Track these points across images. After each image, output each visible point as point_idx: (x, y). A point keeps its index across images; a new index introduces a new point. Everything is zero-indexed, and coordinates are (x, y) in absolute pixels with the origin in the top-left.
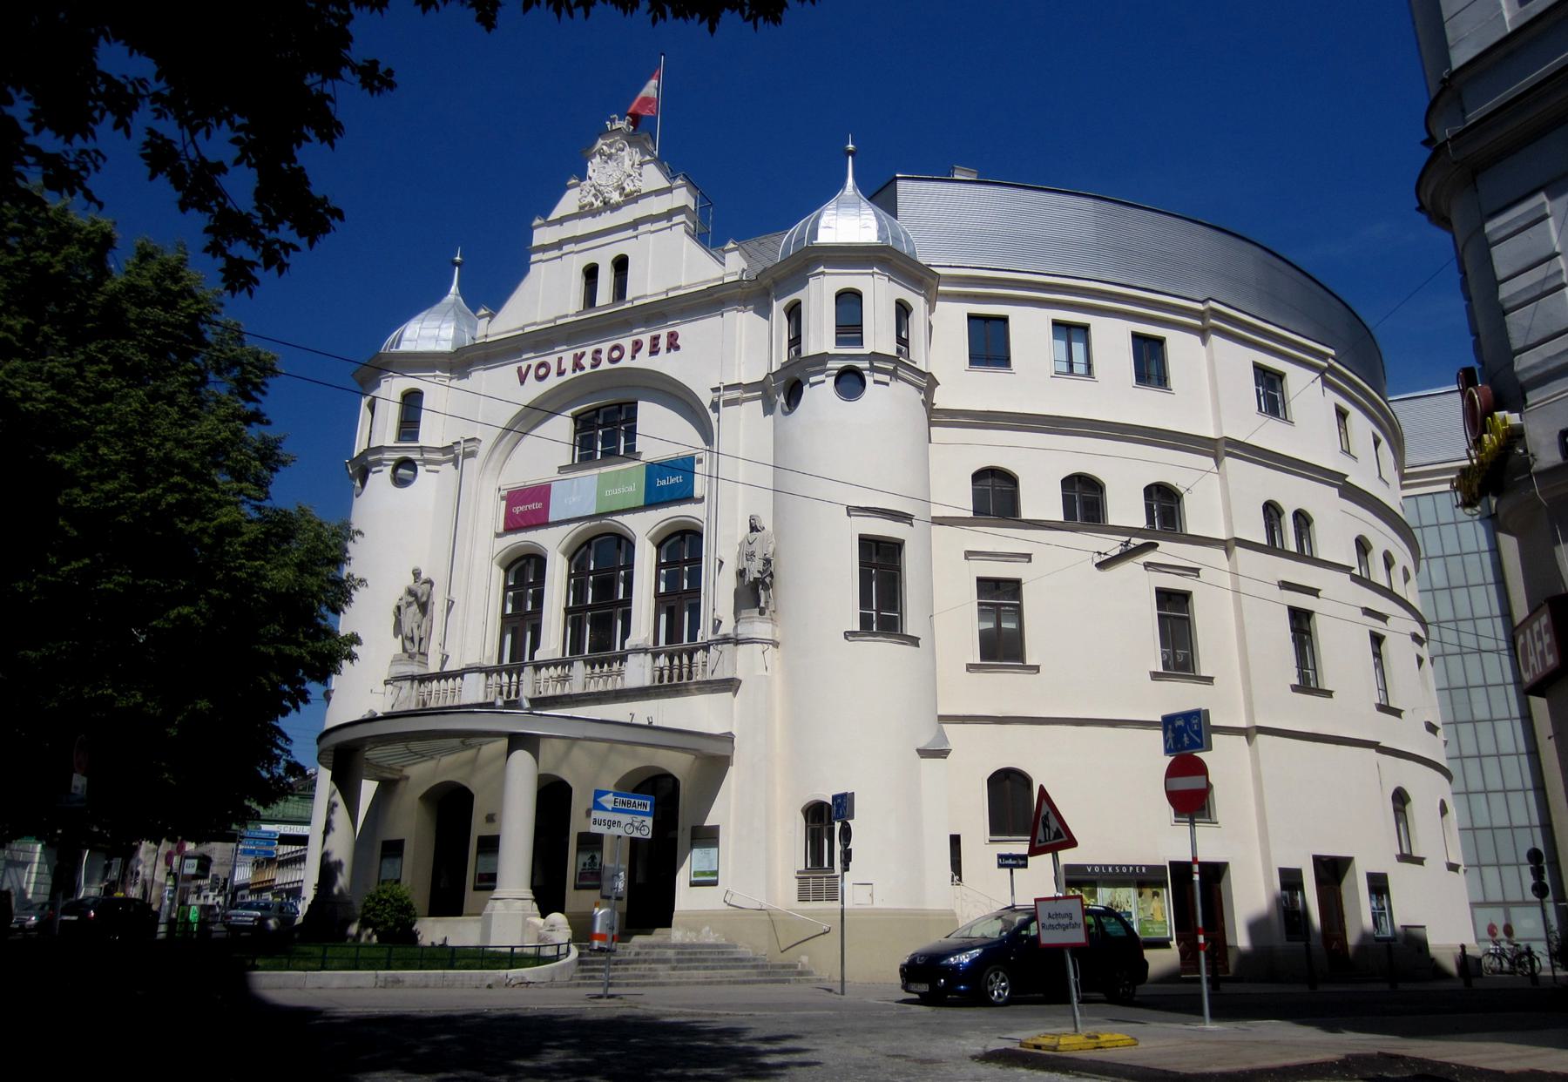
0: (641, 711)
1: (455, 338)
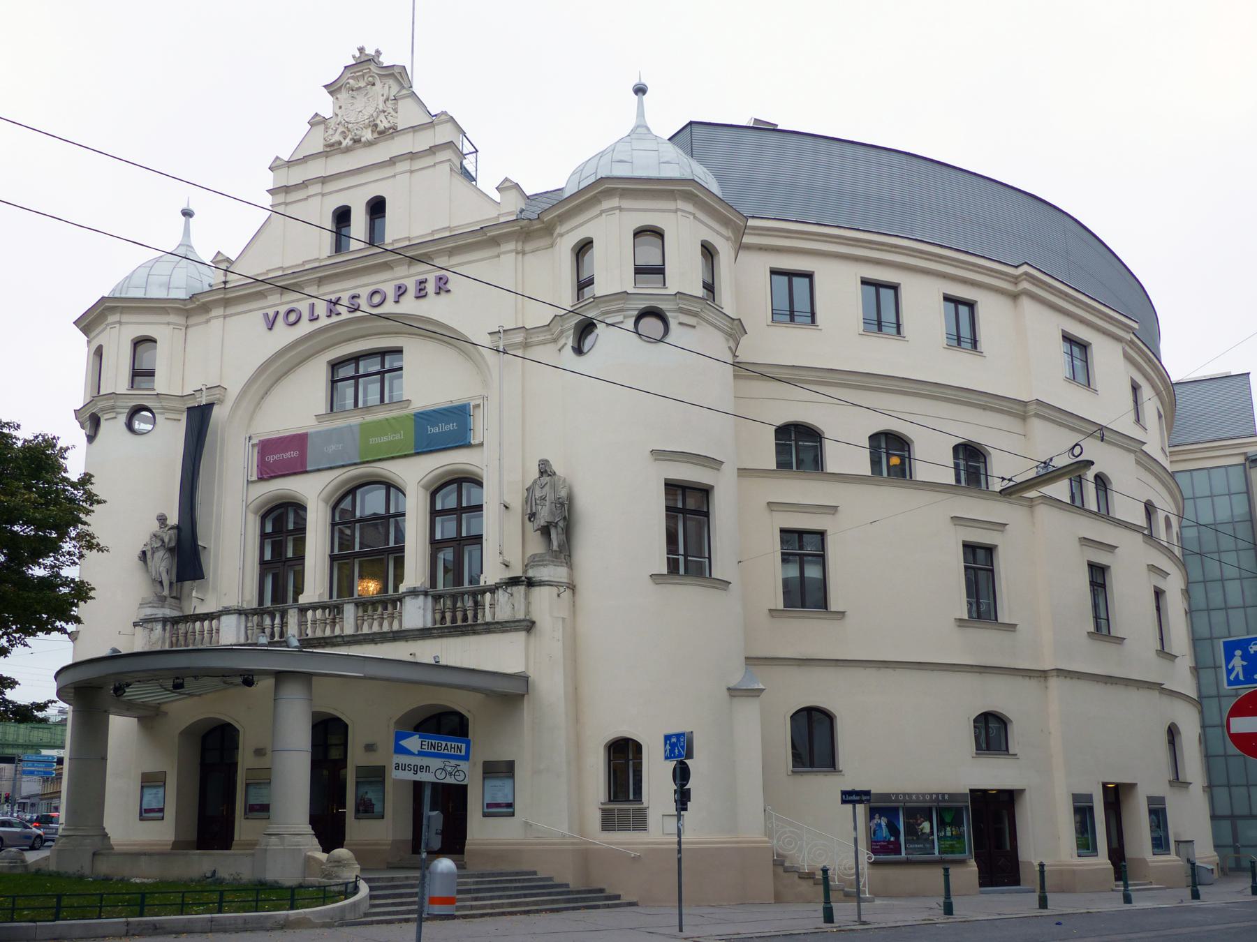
0: (425, 651)
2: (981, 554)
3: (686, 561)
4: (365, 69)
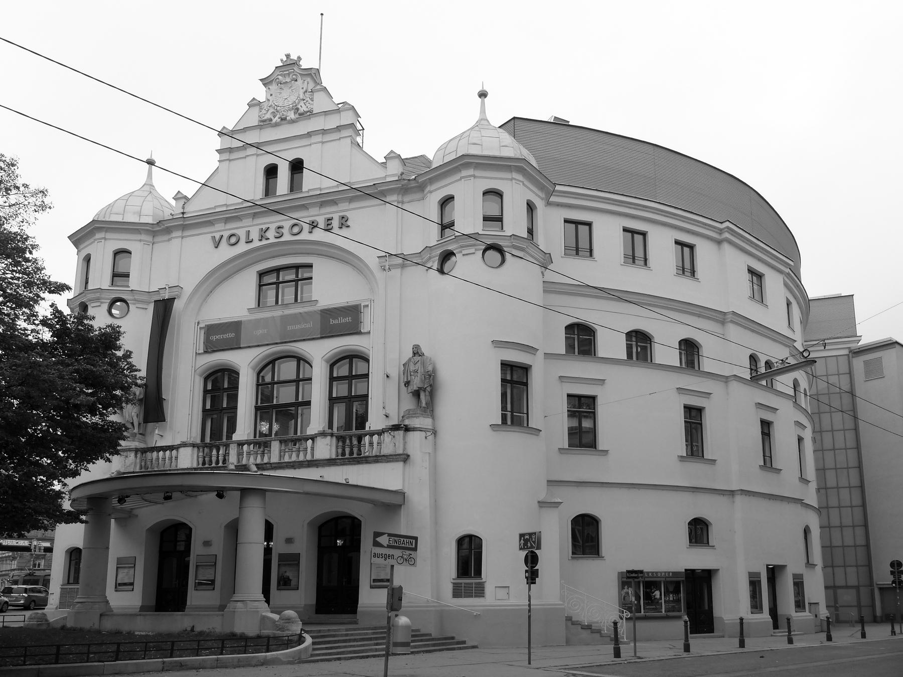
2: (694, 413)
3: (512, 416)
4: (290, 69)
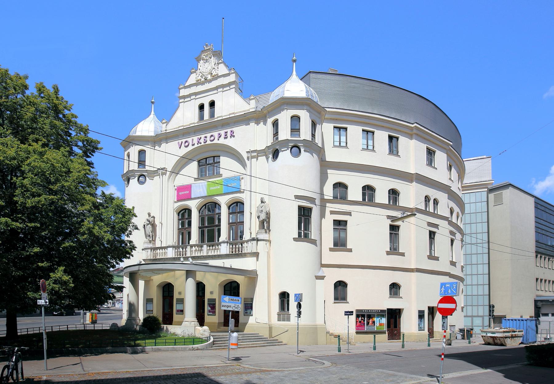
1: (155, 131)
